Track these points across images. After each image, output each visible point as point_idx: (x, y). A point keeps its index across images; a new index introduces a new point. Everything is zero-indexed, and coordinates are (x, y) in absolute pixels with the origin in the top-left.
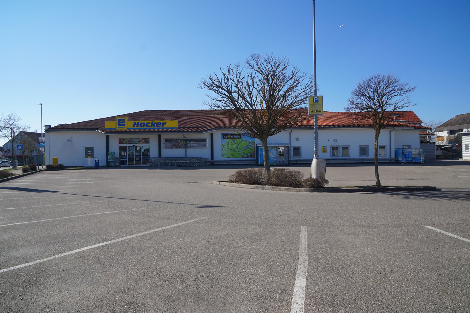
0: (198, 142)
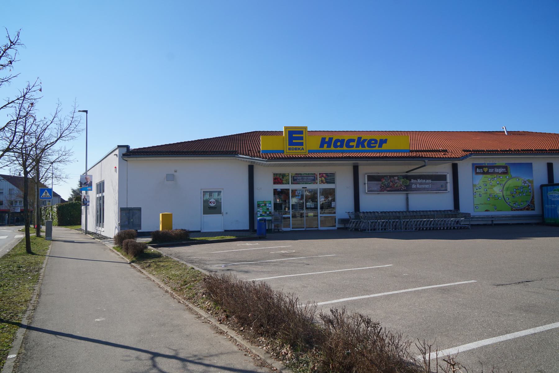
0: (430, 181)
